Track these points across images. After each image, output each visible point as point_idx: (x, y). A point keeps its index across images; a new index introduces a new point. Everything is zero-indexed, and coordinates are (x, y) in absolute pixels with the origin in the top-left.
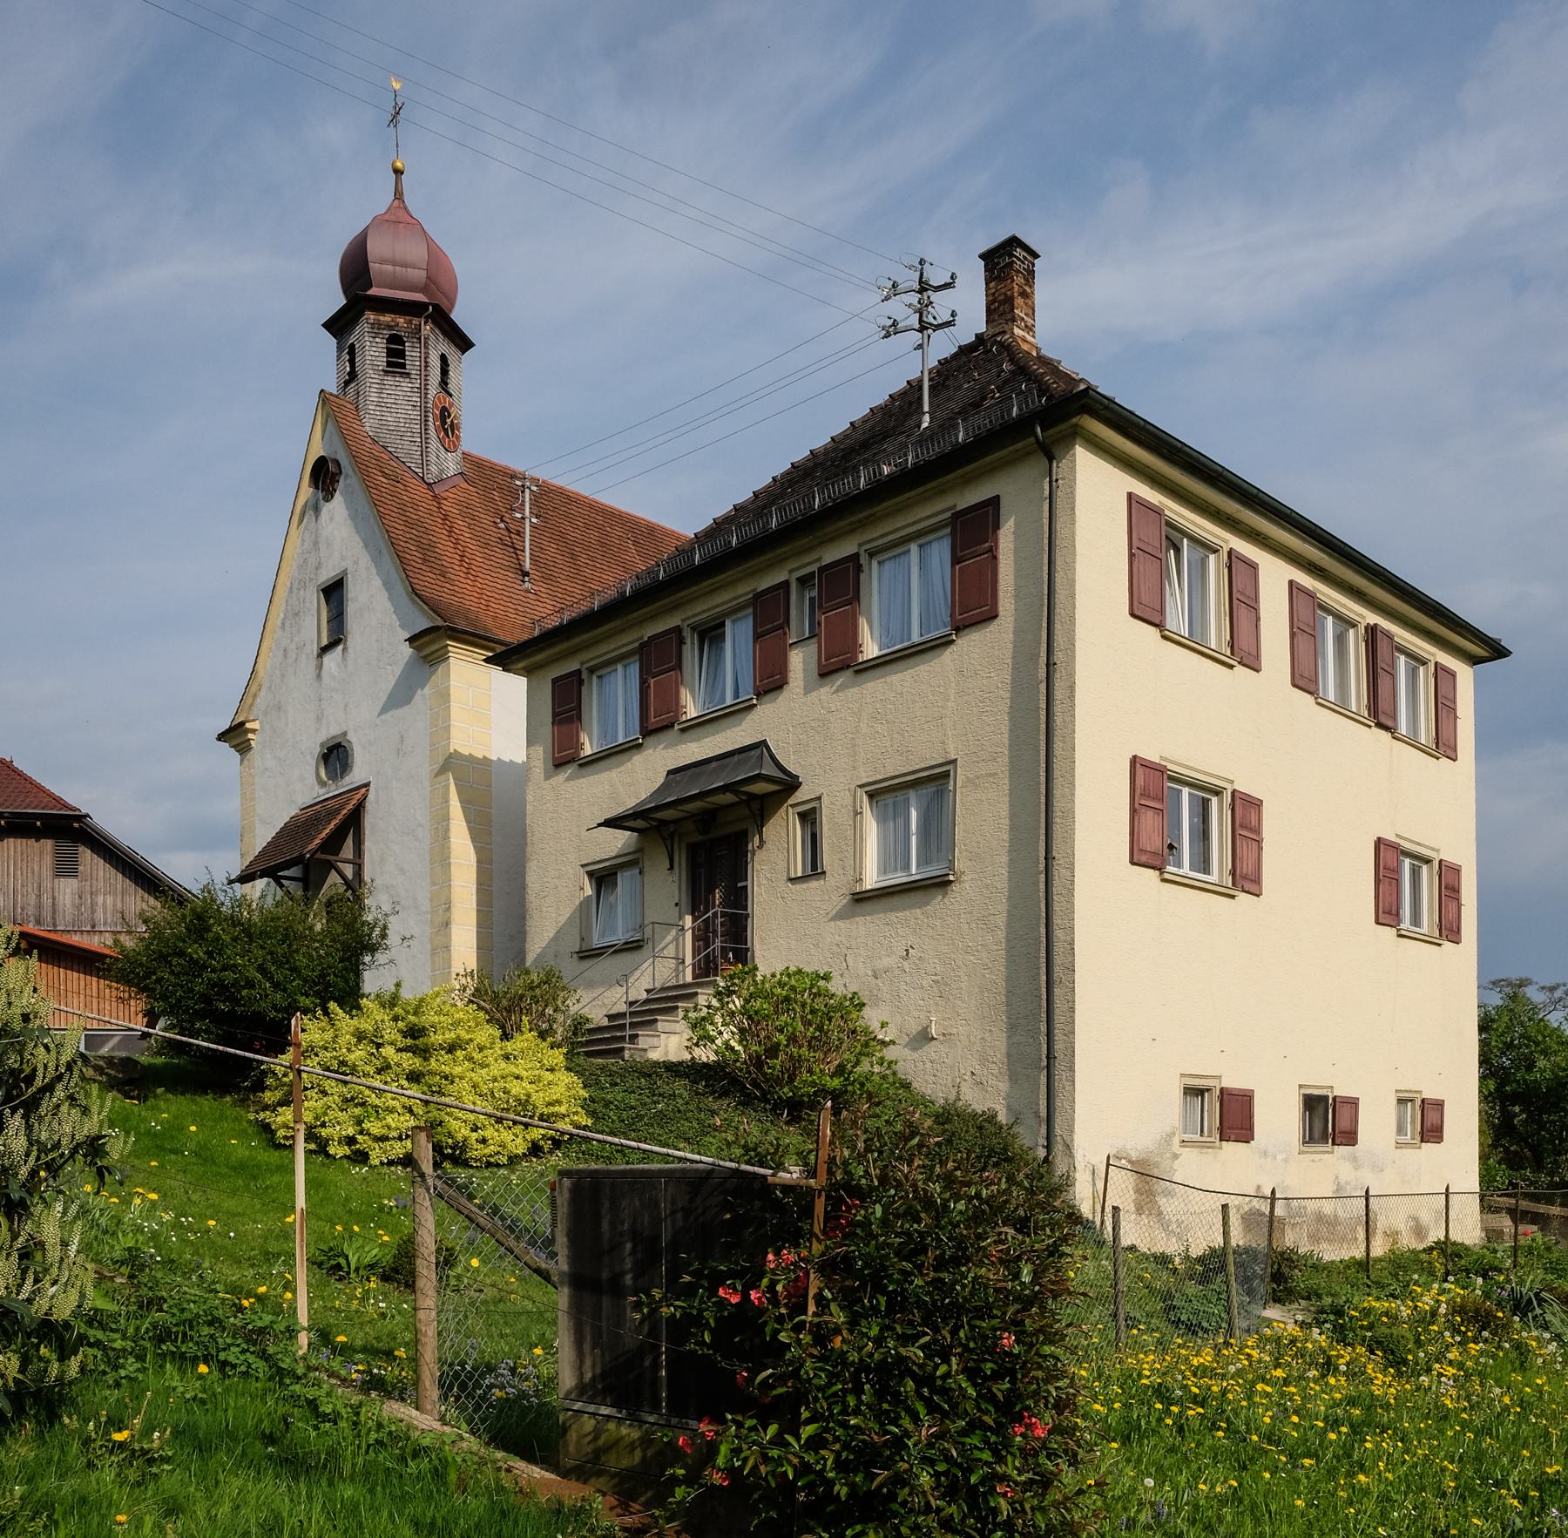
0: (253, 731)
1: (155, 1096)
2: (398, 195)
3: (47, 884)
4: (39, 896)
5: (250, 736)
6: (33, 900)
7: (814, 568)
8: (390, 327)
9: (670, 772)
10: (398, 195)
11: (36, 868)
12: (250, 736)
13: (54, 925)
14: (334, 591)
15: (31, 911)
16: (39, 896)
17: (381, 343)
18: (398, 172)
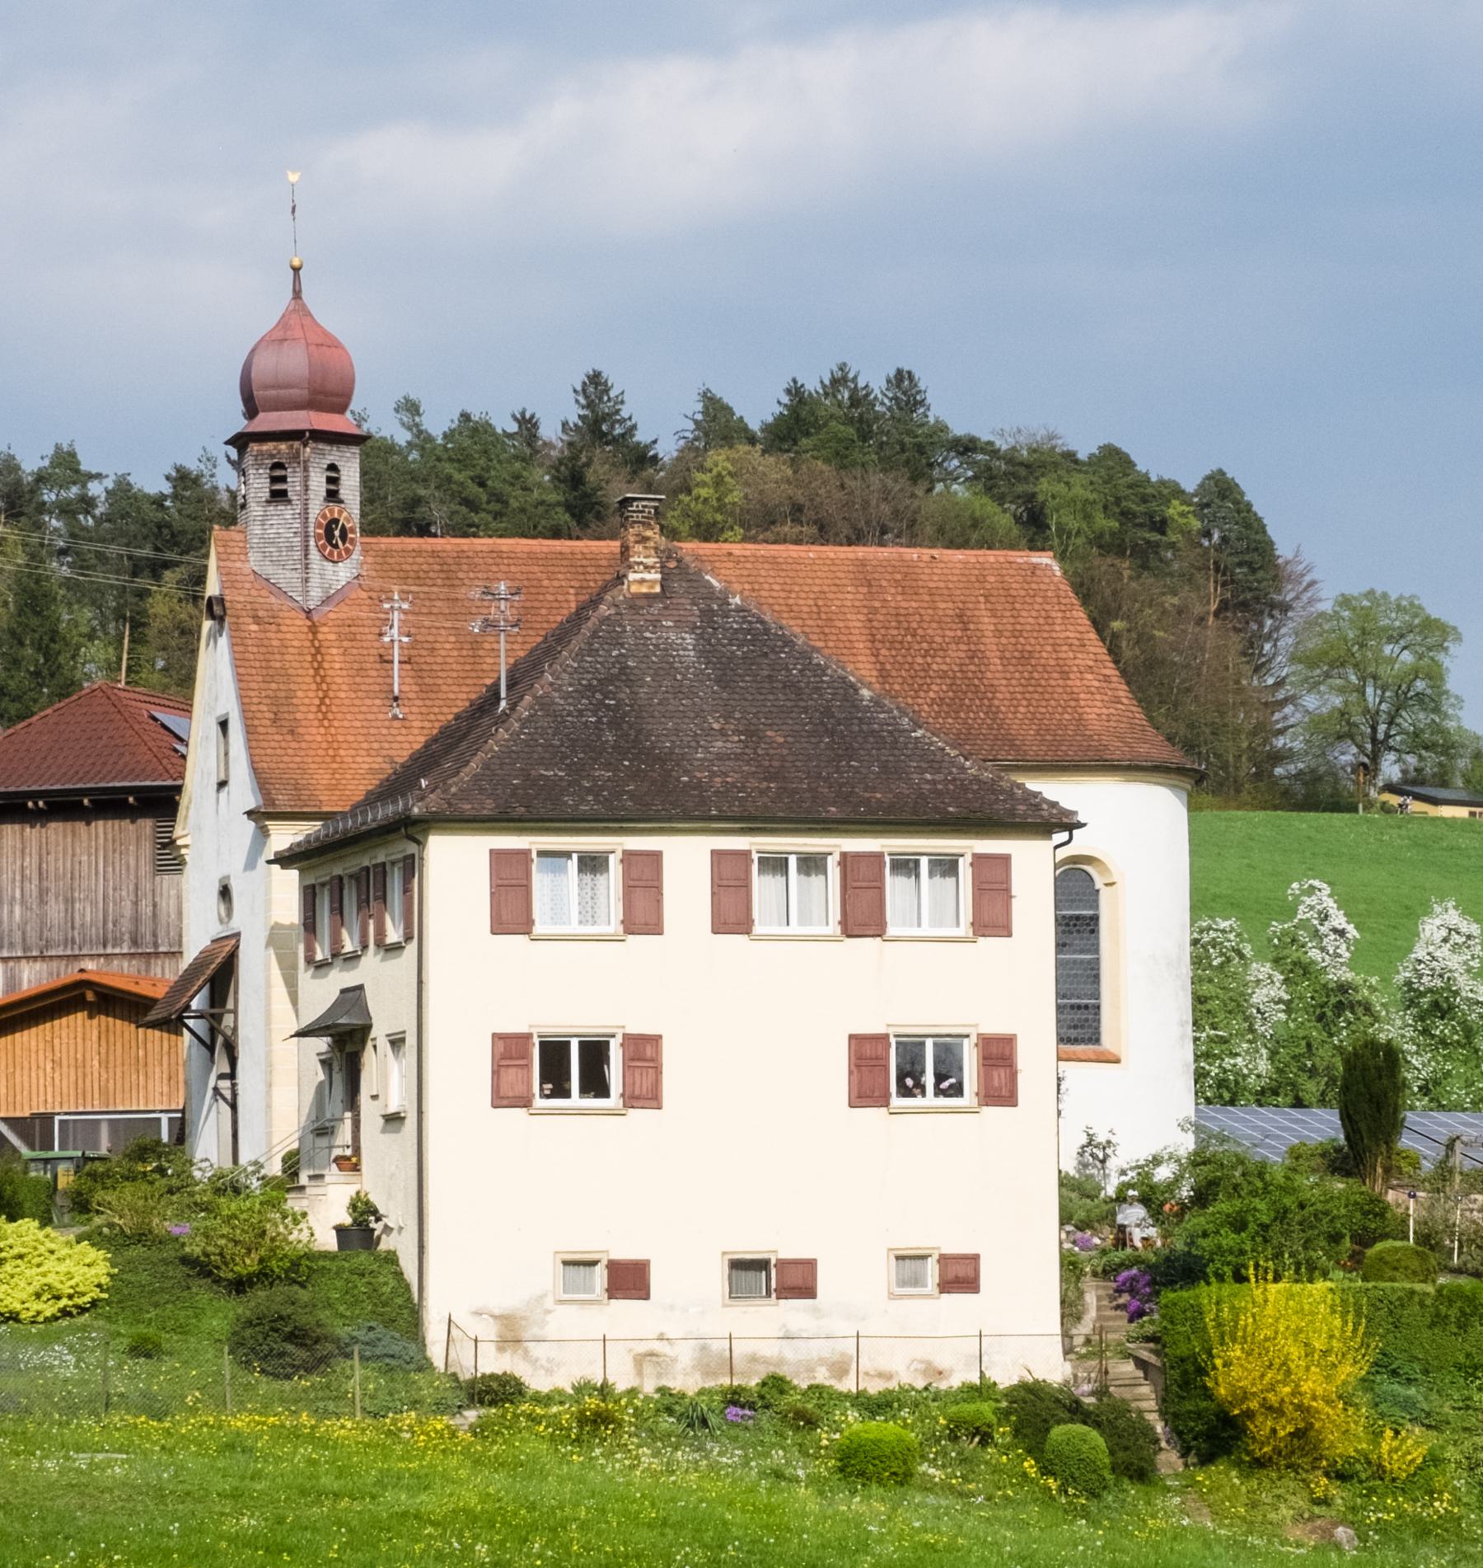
0: (186, 846)
1: (15, 1193)
2: (297, 294)
3: (146, 885)
4: (136, 903)
5: (183, 851)
6: (127, 909)
7: (400, 856)
8: (272, 456)
9: (343, 991)
10: (297, 294)
11: (132, 862)
12: (183, 851)
13: (156, 945)
14: (224, 725)
15: (126, 926)
16: (136, 903)
17: (264, 472)
18: (296, 270)
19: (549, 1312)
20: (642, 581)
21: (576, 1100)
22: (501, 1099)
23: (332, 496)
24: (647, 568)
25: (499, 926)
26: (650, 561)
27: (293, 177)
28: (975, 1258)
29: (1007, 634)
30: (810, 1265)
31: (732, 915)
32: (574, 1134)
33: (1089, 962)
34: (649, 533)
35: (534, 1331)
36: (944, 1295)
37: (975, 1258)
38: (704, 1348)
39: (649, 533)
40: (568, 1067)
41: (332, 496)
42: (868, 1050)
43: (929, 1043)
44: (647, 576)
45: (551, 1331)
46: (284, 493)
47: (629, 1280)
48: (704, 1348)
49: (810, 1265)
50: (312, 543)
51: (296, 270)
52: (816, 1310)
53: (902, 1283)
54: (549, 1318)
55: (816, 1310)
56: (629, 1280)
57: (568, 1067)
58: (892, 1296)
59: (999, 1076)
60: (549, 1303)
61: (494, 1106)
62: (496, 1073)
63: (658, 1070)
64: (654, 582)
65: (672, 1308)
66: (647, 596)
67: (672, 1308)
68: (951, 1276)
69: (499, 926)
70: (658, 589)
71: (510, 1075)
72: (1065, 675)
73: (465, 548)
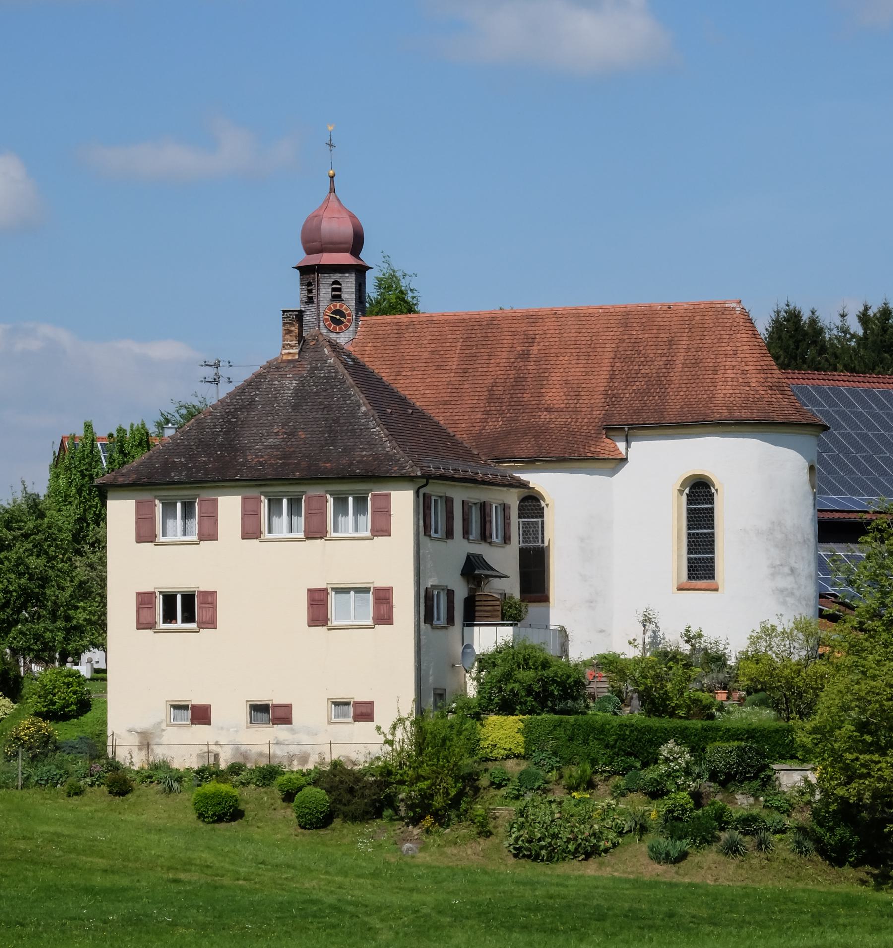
2: (333, 190)
10: (333, 190)
19: (164, 730)
20: (289, 353)
21: (179, 624)
22: (142, 625)
23: (337, 298)
24: (292, 347)
25: (140, 539)
26: (293, 343)
27: (331, 128)
28: (371, 703)
29: (692, 350)
30: (289, 707)
31: (251, 532)
32: (178, 642)
33: (709, 534)
34: (293, 328)
35: (157, 740)
36: (356, 723)
37: (371, 703)
38: (237, 749)
39: (293, 328)
40: (185, 608)
41: (337, 298)
42: (317, 596)
43: (179, 598)
44: (291, 351)
45: (164, 740)
46: (339, 296)
47: (201, 715)
48: (237, 749)
49: (289, 707)
50: (322, 324)
51: (332, 177)
52: (292, 730)
53: (337, 716)
54: (164, 733)
55: (292, 730)
56: (201, 715)
57: (185, 608)
58: (330, 723)
59: (384, 609)
60: (164, 726)
61: (138, 629)
62: (138, 612)
63: (214, 608)
64: (294, 353)
65: (222, 728)
66: (289, 362)
67: (222, 728)
68: (358, 712)
69: (140, 539)
70: (297, 357)
71: (145, 613)
72: (715, 372)
73: (414, 320)
